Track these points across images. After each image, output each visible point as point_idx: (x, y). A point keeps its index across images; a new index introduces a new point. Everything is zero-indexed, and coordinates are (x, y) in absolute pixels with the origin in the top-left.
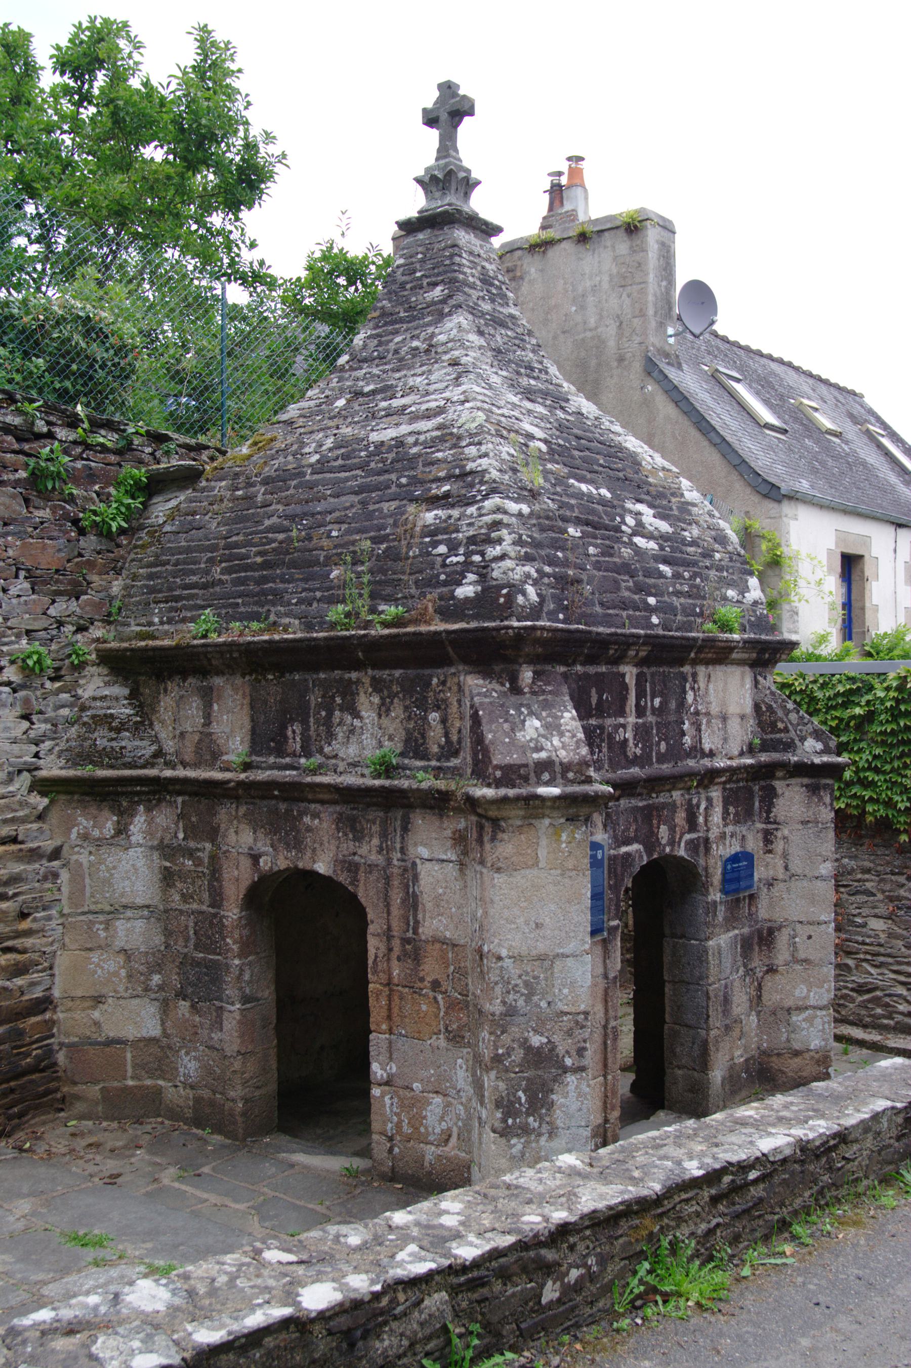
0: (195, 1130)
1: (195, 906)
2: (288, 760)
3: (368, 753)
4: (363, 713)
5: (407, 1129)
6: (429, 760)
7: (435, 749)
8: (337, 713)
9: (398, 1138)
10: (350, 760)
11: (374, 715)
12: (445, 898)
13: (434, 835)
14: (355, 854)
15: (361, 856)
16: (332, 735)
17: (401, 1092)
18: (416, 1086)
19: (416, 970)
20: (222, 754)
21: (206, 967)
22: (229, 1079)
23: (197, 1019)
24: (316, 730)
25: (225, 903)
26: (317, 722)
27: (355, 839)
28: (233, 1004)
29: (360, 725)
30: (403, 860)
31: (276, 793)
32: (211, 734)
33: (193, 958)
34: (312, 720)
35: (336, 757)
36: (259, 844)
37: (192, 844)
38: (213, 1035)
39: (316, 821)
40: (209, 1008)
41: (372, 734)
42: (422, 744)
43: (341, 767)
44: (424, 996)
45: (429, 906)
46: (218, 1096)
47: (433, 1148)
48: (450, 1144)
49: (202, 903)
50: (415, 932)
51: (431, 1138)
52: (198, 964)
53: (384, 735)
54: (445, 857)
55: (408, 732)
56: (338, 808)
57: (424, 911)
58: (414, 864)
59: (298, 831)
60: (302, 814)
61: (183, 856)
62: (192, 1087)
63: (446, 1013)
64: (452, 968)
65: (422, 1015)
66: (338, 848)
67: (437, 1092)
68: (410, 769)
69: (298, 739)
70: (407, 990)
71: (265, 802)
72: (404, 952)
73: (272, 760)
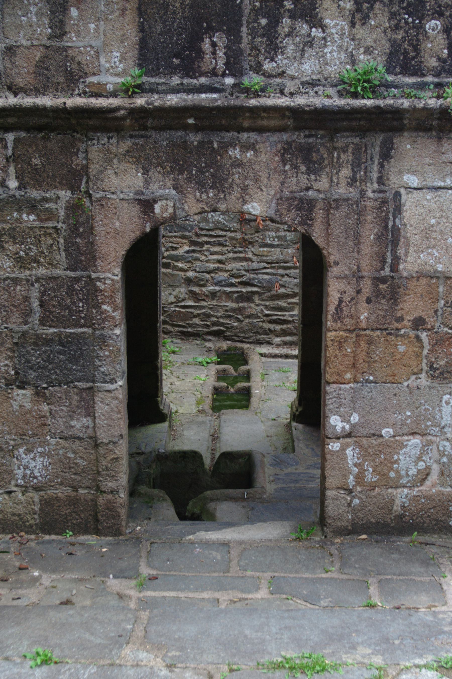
0: (47, 537)
1: (42, 271)
2: (203, 80)
3: (331, 70)
4: (327, 21)
5: (369, 477)
6: (423, 75)
7: (433, 63)
8: (286, 21)
9: (359, 489)
10: (305, 79)
11: (344, 24)
12: (437, 229)
13: (427, 160)
14: (308, 189)
15: (319, 191)
16: (276, 48)
17: (365, 441)
18: (387, 432)
19: (392, 309)
20: (86, 75)
21: (61, 343)
22: (107, 469)
23: (45, 408)
24: (251, 43)
25: (99, 262)
26: (253, 33)
27: (309, 172)
28: (113, 381)
29: (321, 35)
30: (380, 192)
31: (191, 121)
32: (66, 49)
33: (38, 336)
34: (244, 29)
35: (282, 74)
36: (154, 187)
37: (34, 194)
38: (73, 423)
39: (250, 154)
40: (66, 393)
41: (341, 47)
42: (413, 58)
43: (290, 86)
44: (402, 336)
45: (415, 239)
46: (81, 491)
47: (406, 491)
48: (428, 483)
49: (55, 267)
50: (394, 268)
51: (404, 481)
52: (48, 341)
53: (357, 47)
54: (442, 184)
55: (393, 43)
56: (285, 136)
57: (408, 245)
58: (397, 195)
59: (220, 167)
60: (224, 146)
61: (19, 210)
62: (37, 489)
63: (431, 351)
64: (443, 302)
65: (399, 356)
66: (282, 183)
67: (413, 434)
68: (396, 87)
69: (220, 54)
70: (378, 333)
71: (166, 134)
72: (378, 294)
73: (176, 80)
